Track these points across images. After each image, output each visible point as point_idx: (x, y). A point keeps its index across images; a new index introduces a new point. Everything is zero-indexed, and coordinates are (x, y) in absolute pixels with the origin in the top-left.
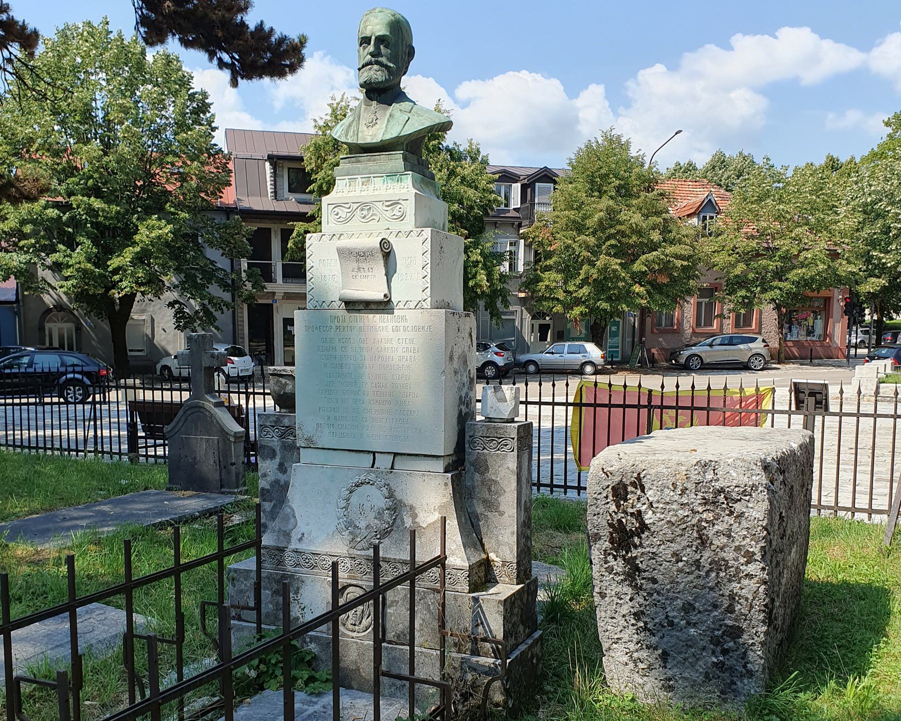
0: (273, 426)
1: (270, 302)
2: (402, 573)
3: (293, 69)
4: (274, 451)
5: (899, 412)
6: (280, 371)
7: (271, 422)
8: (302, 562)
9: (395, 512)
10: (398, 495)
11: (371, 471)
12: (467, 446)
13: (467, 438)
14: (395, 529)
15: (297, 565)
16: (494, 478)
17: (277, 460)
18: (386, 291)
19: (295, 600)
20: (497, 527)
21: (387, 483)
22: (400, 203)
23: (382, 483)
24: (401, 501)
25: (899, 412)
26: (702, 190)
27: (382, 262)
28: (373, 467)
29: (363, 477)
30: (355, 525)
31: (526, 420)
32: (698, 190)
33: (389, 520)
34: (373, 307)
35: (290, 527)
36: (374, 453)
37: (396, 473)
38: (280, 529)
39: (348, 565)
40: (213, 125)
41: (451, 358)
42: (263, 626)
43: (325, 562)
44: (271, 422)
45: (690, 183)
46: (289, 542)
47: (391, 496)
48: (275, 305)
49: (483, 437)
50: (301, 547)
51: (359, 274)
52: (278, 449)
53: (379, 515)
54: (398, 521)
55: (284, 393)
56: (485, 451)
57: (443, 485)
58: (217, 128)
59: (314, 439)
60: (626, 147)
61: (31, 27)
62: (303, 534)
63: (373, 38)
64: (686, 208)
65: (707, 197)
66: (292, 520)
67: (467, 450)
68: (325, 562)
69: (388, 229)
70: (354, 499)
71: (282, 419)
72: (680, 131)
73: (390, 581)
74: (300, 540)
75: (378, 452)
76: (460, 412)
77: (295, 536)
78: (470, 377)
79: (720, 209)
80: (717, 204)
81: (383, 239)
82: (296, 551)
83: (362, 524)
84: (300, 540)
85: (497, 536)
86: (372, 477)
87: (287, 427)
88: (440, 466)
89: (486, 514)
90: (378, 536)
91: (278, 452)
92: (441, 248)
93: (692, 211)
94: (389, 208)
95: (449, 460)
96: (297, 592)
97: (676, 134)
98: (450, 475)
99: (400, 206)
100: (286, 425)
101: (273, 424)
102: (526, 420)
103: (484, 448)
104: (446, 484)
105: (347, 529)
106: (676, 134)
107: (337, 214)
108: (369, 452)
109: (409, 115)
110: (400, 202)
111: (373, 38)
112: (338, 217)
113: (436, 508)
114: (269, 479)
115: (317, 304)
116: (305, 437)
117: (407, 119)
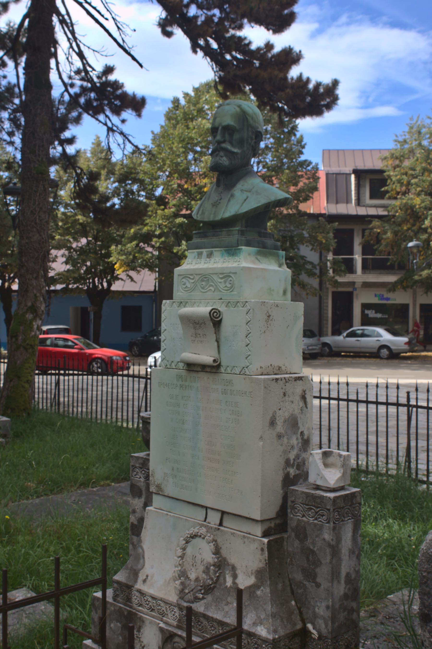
1: (350, 289)
2: (218, 633)
3: (329, 107)
4: (141, 491)
8: (144, 603)
9: (219, 569)
10: (224, 552)
12: (289, 511)
13: (289, 503)
14: (218, 586)
15: (141, 605)
16: (311, 547)
18: (217, 356)
19: (137, 637)
20: (313, 598)
22: (230, 276)
23: (211, 538)
24: (225, 559)
27: (213, 329)
29: (196, 530)
30: (187, 576)
33: (213, 577)
35: (139, 566)
36: (206, 508)
37: (222, 531)
38: (132, 567)
39: (177, 614)
40: (303, 143)
41: (272, 423)
42: (184, 635)
43: (160, 607)
46: (136, 581)
47: (217, 552)
48: (355, 293)
50: (145, 588)
53: (206, 571)
54: (221, 579)
56: (304, 519)
57: (260, 550)
58: (305, 144)
59: (162, 487)
61: (121, 82)
62: (147, 576)
63: (220, 128)
66: (141, 561)
67: (289, 515)
68: (160, 607)
69: (221, 299)
70: (189, 550)
73: (209, 639)
74: (144, 581)
76: (287, 476)
77: (141, 577)
78: (302, 439)
81: (213, 309)
82: (139, 591)
83: (193, 576)
84: (144, 581)
85: (314, 607)
86: (203, 530)
88: (258, 530)
89: (305, 583)
90: (203, 592)
92: (269, 316)
94: (222, 281)
95: (266, 526)
96: (139, 631)
98: (266, 540)
99: (230, 279)
103: (304, 516)
104: (262, 550)
105: (180, 579)
107: (184, 284)
108: (202, 506)
109: (249, 194)
110: (231, 275)
111: (220, 128)
112: (185, 286)
113: (253, 572)
117: (245, 197)
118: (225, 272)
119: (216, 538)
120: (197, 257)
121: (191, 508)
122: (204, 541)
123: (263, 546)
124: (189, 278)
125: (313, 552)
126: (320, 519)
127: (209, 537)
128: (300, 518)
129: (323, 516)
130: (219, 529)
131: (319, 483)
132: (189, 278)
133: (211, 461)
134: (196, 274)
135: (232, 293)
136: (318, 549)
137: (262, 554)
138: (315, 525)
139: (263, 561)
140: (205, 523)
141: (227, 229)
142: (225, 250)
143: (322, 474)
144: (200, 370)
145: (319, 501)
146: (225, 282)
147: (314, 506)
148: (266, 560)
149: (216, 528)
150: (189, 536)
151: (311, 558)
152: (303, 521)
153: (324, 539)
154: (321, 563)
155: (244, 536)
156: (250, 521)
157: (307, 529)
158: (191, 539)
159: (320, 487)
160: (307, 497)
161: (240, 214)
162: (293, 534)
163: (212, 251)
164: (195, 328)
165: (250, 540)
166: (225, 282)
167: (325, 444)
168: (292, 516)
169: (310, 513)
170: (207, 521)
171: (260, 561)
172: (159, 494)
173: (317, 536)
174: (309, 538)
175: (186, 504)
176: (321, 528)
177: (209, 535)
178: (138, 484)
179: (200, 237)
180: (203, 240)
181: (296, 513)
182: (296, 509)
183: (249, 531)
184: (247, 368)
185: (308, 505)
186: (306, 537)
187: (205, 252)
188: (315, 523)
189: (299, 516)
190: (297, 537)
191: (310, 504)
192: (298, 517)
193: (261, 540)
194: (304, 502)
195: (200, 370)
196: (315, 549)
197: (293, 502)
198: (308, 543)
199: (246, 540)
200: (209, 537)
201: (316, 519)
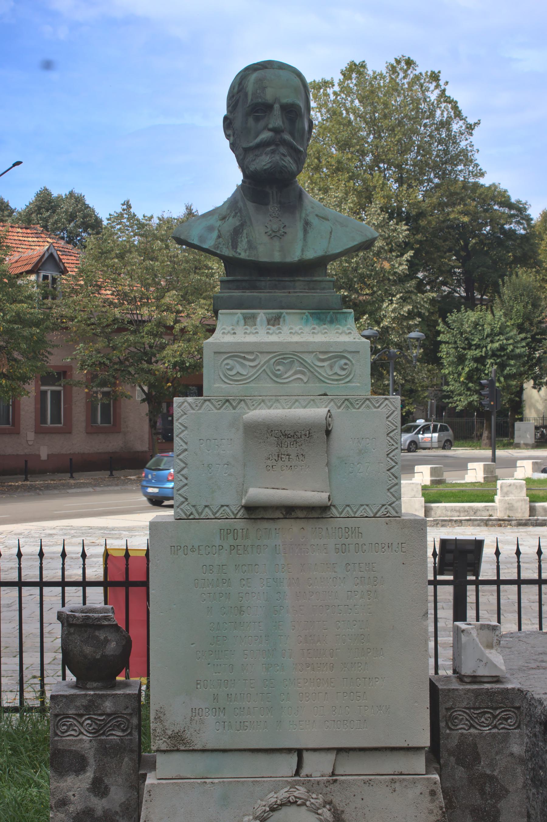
0: (81, 716)
5: (544, 576)
6: (99, 619)
7: (77, 708)
11: (298, 783)
16: (488, 772)
17: (90, 774)
21: (328, 799)
23: (320, 801)
25: (544, 576)
26: (35, 239)
28: (297, 773)
31: (84, 603)
32: (30, 239)
34: (300, 514)
36: (300, 752)
37: (343, 782)
44: (77, 708)
45: (19, 230)
49: (469, 708)
51: (280, 463)
52: (91, 756)
55: (103, 656)
59: (187, 735)
60: (50, 194)
64: (19, 264)
65: (48, 250)
67: (442, 731)
69: (325, 395)
71: (99, 701)
72: (18, 163)
75: (307, 750)
79: (65, 268)
80: (60, 259)
86: (301, 792)
87: (109, 715)
91: (91, 761)
93: (29, 268)
94: (325, 364)
97: (14, 165)
99: (344, 361)
100: (108, 711)
101: (81, 712)
102: (84, 603)
104: (433, 793)
106: (14, 165)
108: (289, 750)
114: (71, 808)
115: (193, 510)
116: (169, 732)
118: (332, 349)
119: (329, 798)
120: (242, 322)
121: (262, 760)
122: (304, 808)
123: (433, 787)
124: (244, 358)
125: (491, 778)
126: (502, 726)
127: (317, 799)
128: (465, 732)
129: (506, 720)
130: (335, 781)
131: (481, 672)
132: (244, 358)
133: (313, 669)
134: (261, 353)
135: (349, 384)
136: (500, 772)
137: (432, 801)
138: (494, 736)
139: (436, 811)
140: (297, 778)
141: (307, 279)
142: (312, 314)
143: (487, 658)
144: (281, 516)
145: (499, 698)
146: (331, 367)
147: (492, 708)
148: (441, 808)
149: (328, 781)
150: (268, 809)
151: (488, 789)
152: (471, 734)
153: (512, 754)
154: (507, 791)
155: (393, 779)
156: (402, 752)
157: (479, 746)
158: (272, 814)
159: (478, 679)
160: (476, 697)
161: (187, 242)
162: (452, 759)
163: (282, 313)
164: (280, 444)
165: (405, 783)
166: (331, 367)
167: (431, 614)
168: (448, 731)
169: (483, 719)
170: (304, 772)
171: (431, 812)
172: (178, 750)
173: (497, 753)
174: (482, 759)
175: (248, 755)
176: (506, 738)
177: (314, 796)
178: (73, 748)
179: (238, 288)
180: (248, 294)
181: (457, 725)
182: (456, 718)
183: (398, 770)
184: (390, 505)
185: (479, 708)
186: (477, 758)
187: (262, 315)
188: (494, 733)
189: (461, 729)
190: (459, 762)
191: (483, 705)
192: (460, 731)
193: (428, 779)
194: (471, 705)
195: (281, 516)
196: (495, 773)
197: (448, 709)
198: (483, 767)
199: (397, 785)
200: (317, 799)
201: (495, 727)
